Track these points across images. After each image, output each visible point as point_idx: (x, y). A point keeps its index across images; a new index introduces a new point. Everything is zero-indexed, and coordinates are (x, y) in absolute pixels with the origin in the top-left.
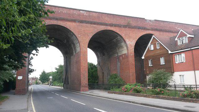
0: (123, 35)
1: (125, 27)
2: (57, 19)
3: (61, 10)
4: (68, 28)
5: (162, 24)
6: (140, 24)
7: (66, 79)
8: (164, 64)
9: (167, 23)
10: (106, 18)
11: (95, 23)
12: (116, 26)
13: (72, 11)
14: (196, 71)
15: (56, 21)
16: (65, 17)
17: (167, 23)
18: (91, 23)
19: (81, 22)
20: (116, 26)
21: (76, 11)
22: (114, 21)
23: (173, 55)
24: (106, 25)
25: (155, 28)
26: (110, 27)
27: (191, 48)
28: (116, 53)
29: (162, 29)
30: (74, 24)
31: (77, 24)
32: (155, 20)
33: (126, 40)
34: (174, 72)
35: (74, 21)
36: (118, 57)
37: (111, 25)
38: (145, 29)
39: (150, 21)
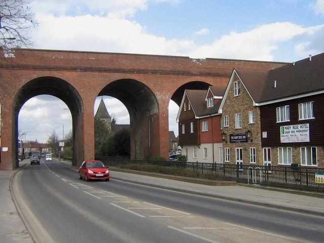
0: (151, 86)
1: (154, 72)
2: (50, 69)
3: (57, 55)
4: (66, 80)
5: (220, 64)
6: (180, 67)
7: (266, 218)
8: (289, 121)
9: (229, 63)
10: (124, 62)
11: (105, 71)
12: (139, 72)
13: (71, 55)
14: (215, 144)
15: (49, 72)
16: (63, 65)
17: (229, 63)
18: (100, 70)
19: (85, 70)
20: (139, 72)
21: (76, 54)
22: (136, 65)
23: (201, 121)
24: (124, 71)
25: (208, 71)
26: (130, 74)
27: (211, 114)
28: (148, 111)
29: (220, 72)
30: (74, 74)
31: (79, 73)
32: (207, 59)
33: (155, 93)
34: (200, 144)
35: (74, 69)
36: (151, 116)
37: (132, 71)
38: (189, 74)
39: (198, 60)
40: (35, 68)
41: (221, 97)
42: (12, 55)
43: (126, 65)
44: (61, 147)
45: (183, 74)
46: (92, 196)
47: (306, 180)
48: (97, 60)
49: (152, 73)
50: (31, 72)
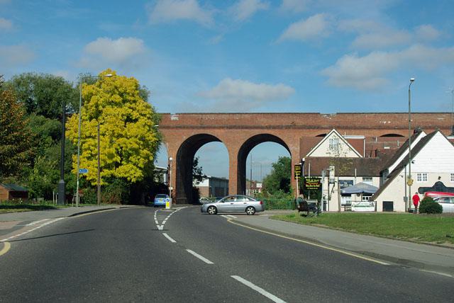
1: (288, 127)
6: (311, 121)
11: (247, 128)
12: (274, 128)
19: (230, 128)
22: (272, 122)
24: (262, 128)
30: (222, 131)
39: (328, 115)
40: (193, 128)
41: (316, 201)
42: (177, 118)
43: (263, 121)
44: (259, 188)
45: (314, 128)
46: (168, 239)
47: (101, 142)
48: (240, 119)
49: (286, 128)
50: (191, 130)
